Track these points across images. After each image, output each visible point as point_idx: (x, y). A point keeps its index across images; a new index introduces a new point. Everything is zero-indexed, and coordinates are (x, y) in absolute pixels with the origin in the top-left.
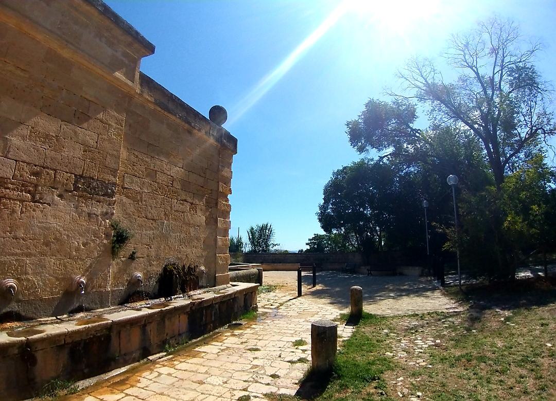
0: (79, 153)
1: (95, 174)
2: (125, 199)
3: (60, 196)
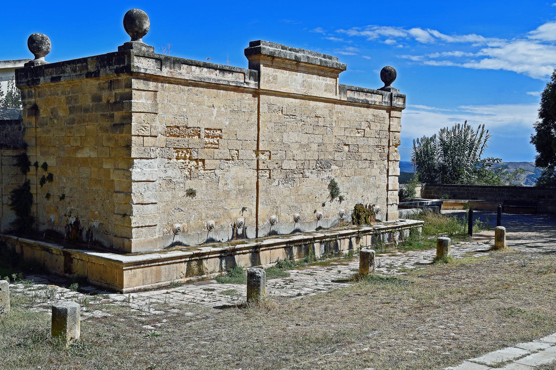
3: (312, 173)
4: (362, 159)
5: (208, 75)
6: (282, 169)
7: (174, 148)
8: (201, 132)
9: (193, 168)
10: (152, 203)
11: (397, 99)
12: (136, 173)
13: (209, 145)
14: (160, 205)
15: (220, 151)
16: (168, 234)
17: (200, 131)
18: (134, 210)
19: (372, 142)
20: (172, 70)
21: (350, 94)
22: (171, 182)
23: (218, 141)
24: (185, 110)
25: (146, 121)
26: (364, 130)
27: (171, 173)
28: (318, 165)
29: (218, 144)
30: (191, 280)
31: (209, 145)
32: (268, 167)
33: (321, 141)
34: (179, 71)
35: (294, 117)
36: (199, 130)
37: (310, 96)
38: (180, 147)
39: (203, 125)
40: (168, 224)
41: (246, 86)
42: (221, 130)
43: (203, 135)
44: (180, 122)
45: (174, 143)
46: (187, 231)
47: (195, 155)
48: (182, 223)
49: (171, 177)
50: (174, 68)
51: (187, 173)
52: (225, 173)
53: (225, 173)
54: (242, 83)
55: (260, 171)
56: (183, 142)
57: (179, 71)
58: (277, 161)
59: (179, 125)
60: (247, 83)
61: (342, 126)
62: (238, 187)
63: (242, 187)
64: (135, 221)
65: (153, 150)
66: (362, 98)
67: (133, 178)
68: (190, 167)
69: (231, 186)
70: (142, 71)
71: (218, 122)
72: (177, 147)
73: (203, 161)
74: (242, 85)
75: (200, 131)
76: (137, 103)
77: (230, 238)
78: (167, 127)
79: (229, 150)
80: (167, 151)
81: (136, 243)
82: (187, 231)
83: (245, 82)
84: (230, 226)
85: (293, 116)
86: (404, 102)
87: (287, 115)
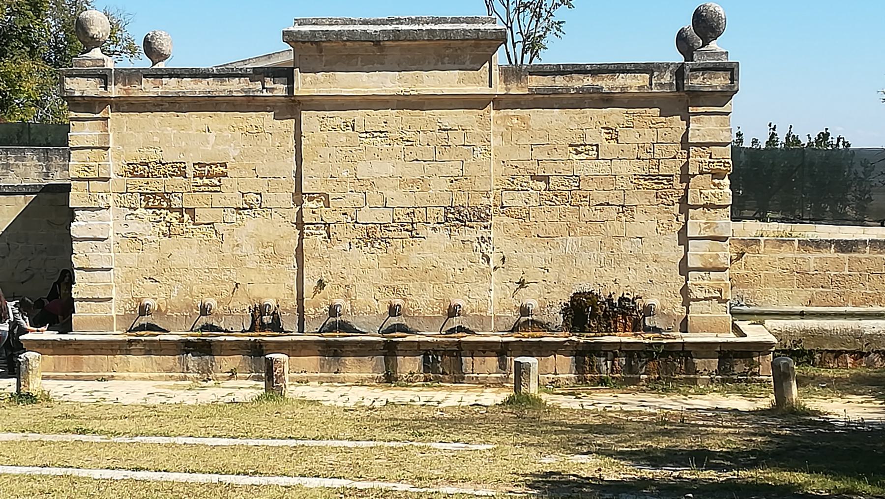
0: (445, 185)
1: (463, 201)
2: (506, 219)
3: (434, 229)
4: (593, 203)
5: (215, 87)
6: (356, 222)
7: (141, 194)
8: (187, 168)
9: (174, 220)
10: (103, 269)
11: (703, 75)
12: (77, 229)
13: (202, 188)
14: (119, 271)
15: (223, 195)
16: (133, 312)
17: (185, 167)
18: (76, 275)
19: (625, 168)
20: (126, 87)
21: (535, 82)
22: (136, 240)
23: (219, 181)
24: (156, 139)
25: (92, 159)
26: (597, 145)
27: (135, 227)
28: (450, 216)
29: (219, 186)
30: (655, 466)
31: (202, 188)
32: (322, 220)
33: (457, 172)
34: (139, 87)
35: (383, 135)
36: (183, 165)
37: (419, 95)
38: (150, 192)
39: (190, 160)
40: (133, 298)
41: (265, 94)
42: (224, 165)
43: (190, 172)
44: (153, 156)
45: (140, 186)
46: (166, 311)
47: (176, 202)
48: (156, 299)
49: (136, 234)
50: (130, 84)
51: (165, 229)
52: (234, 228)
53: (234, 228)
54: (258, 91)
55: (306, 226)
56: (157, 185)
57: (139, 87)
58: (344, 210)
59: (147, 161)
60: (272, 90)
61: (524, 141)
62: (261, 250)
63: (270, 250)
64: (77, 291)
65: (102, 197)
66: (578, 84)
67: (690, 265)
68: (169, 220)
69: (248, 248)
70: (77, 94)
71: (218, 153)
72: (145, 191)
73: (192, 211)
74: (259, 94)
75: (185, 167)
76: (76, 137)
77: (247, 328)
78: (128, 164)
79: (243, 194)
80: (130, 197)
81: (80, 312)
82: (166, 311)
83: (263, 88)
84: (247, 310)
85: (381, 132)
86: (732, 79)
87: (366, 132)
